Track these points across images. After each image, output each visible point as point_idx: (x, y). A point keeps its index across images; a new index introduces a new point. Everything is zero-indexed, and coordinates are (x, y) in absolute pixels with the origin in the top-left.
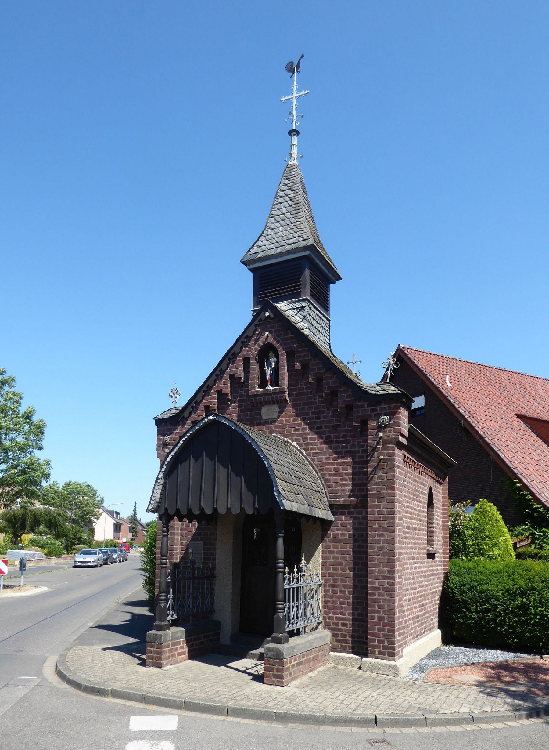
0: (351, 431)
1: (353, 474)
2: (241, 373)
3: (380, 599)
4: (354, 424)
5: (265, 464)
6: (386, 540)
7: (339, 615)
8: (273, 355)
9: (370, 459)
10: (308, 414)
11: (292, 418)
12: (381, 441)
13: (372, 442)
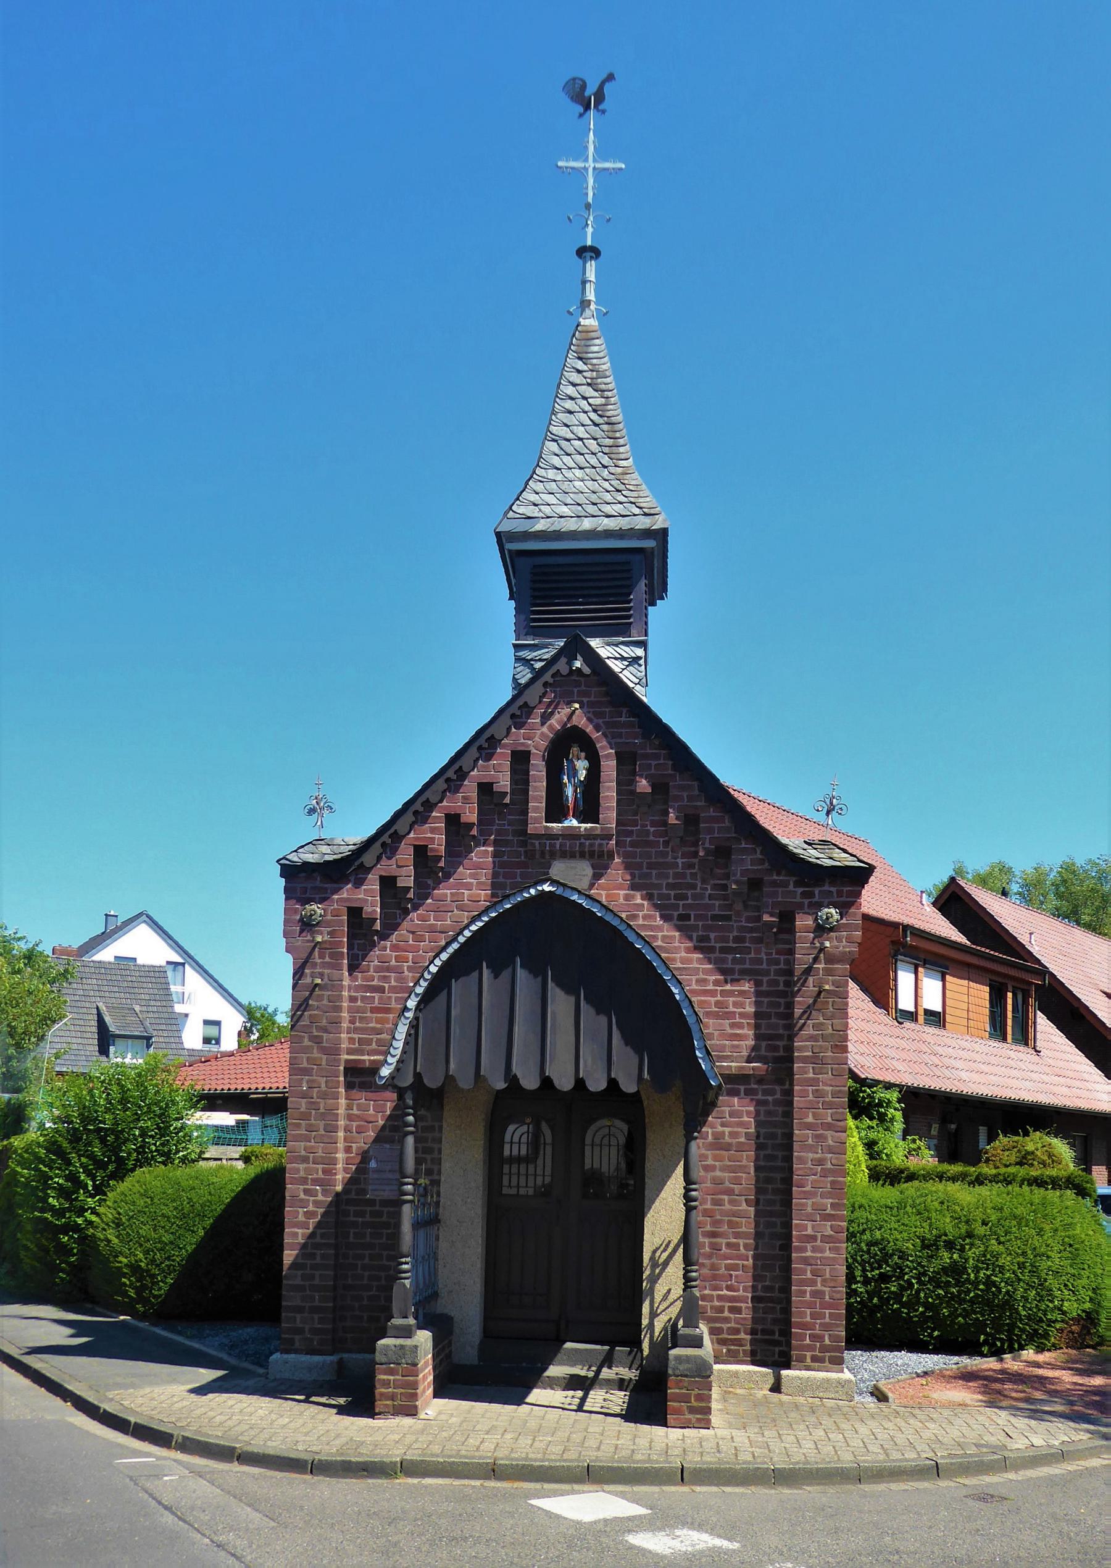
0: (751, 930)
1: (757, 1015)
2: (504, 782)
3: (817, 1258)
4: (766, 918)
5: (673, 994)
6: (829, 1146)
7: (725, 1292)
8: (583, 755)
9: (799, 990)
10: (658, 887)
11: (622, 892)
12: (822, 955)
13: (802, 956)
